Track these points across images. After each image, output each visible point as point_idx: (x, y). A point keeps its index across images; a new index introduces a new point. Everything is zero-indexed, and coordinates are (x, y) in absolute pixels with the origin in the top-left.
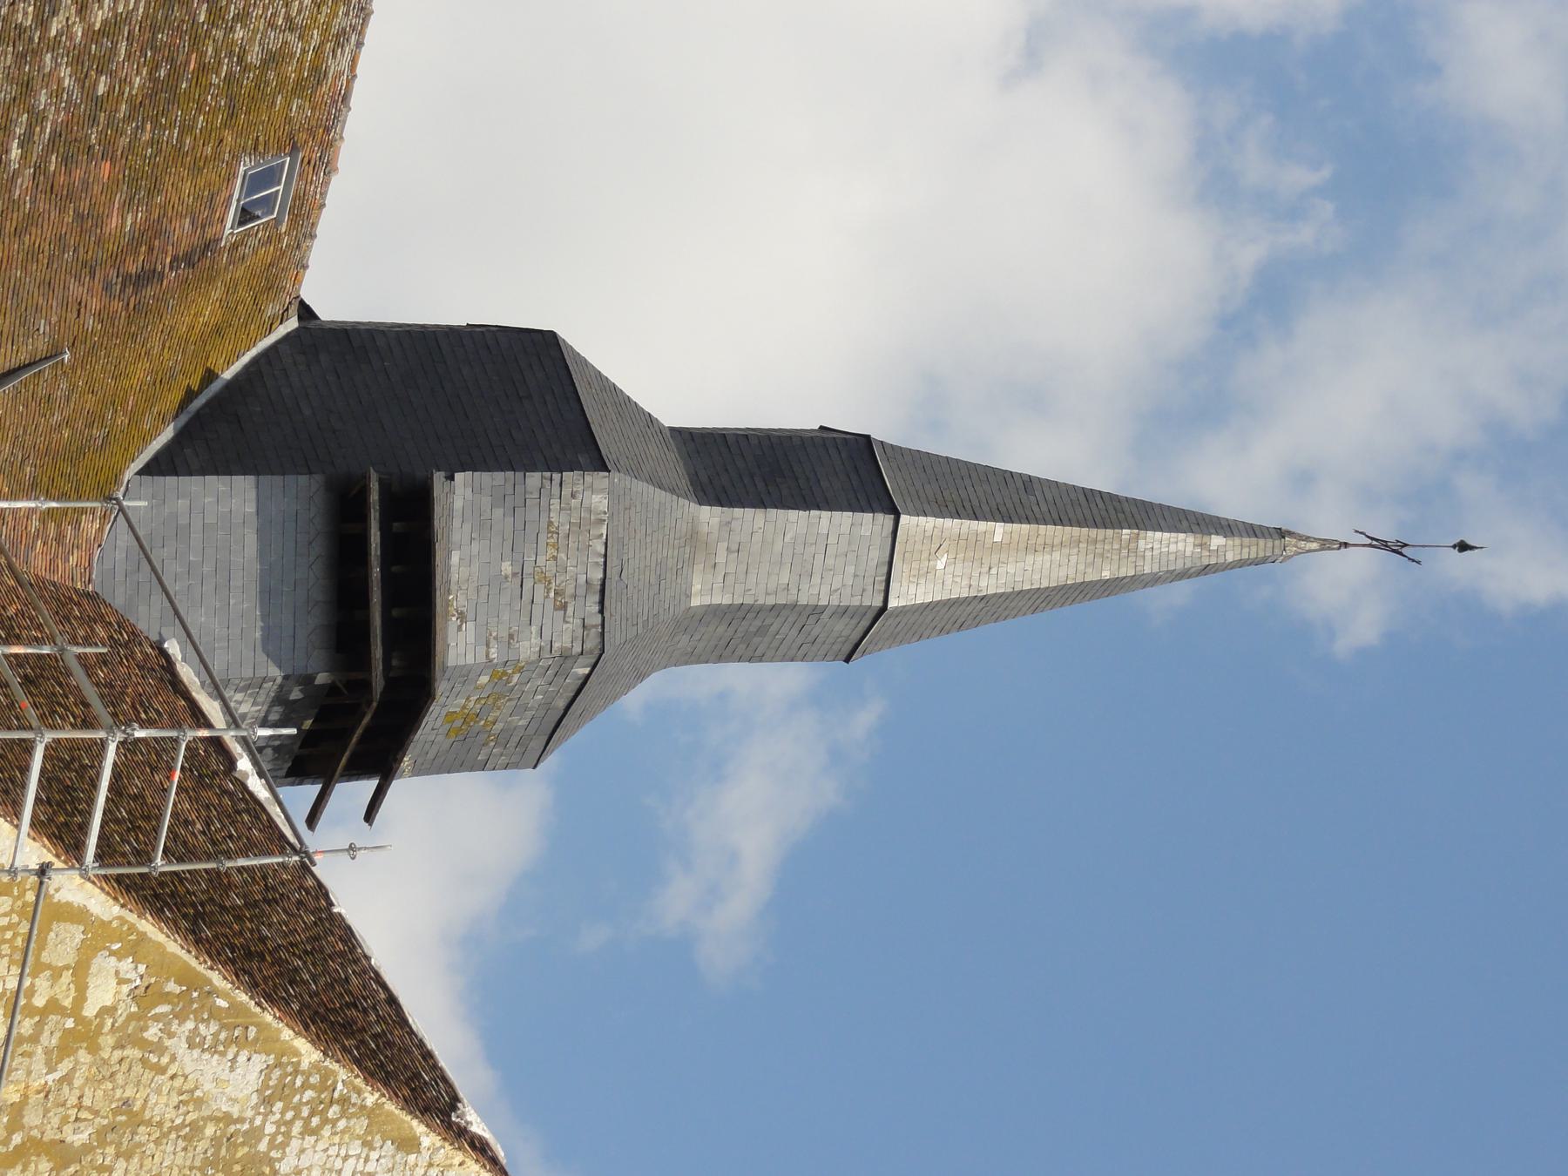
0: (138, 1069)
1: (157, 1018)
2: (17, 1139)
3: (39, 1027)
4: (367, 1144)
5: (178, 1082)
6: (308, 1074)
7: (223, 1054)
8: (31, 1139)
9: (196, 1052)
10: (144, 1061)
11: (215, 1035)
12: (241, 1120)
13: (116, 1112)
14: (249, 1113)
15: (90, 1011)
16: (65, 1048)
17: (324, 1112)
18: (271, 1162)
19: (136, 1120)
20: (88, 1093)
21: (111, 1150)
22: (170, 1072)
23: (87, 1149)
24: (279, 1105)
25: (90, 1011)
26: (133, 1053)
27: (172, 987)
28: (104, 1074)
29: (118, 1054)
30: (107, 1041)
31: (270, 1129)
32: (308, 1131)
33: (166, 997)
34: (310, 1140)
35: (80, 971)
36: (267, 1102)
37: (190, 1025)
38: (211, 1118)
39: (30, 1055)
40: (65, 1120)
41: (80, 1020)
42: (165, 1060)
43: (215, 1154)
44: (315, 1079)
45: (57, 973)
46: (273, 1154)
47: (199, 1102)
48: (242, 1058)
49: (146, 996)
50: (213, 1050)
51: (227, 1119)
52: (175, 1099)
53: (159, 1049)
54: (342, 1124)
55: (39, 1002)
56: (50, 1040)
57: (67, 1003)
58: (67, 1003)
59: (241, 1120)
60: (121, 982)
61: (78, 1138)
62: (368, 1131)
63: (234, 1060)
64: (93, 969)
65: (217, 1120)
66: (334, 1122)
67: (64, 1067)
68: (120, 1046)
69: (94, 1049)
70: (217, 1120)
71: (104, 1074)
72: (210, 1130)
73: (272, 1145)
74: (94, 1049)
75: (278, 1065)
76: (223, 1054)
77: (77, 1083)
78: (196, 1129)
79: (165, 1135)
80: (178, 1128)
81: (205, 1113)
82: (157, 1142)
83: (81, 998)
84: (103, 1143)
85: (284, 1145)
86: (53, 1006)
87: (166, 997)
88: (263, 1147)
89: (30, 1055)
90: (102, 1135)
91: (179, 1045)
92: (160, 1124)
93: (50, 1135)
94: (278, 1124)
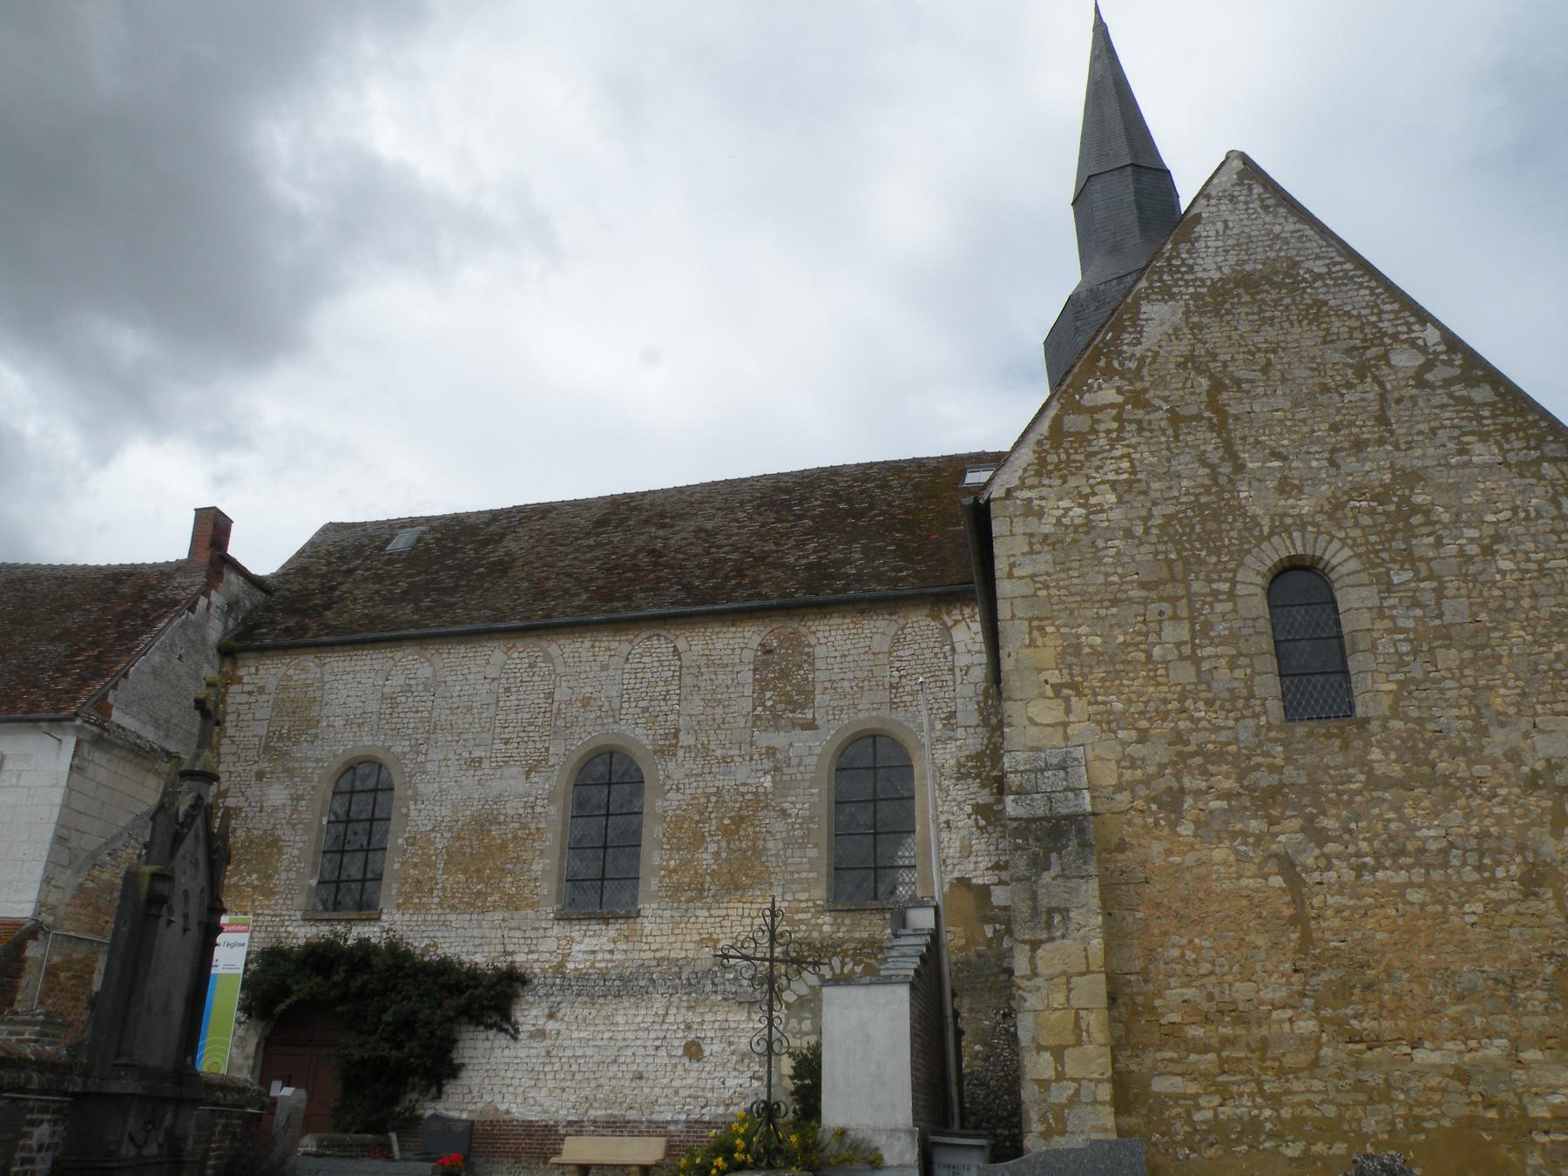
0: (1155, 366)
1: (1122, 364)
2: (1207, 414)
3: (1130, 421)
4: (1197, 240)
5: (1163, 343)
6: (1152, 282)
7: (1142, 326)
8: (1207, 407)
9: (1143, 340)
10: (1150, 364)
11: (1130, 333)
12: (1187, 306)
13: (1186, 368)
14: (1182, 303)
15: (1120, 399)
16: (1147, 405)
17: (1178, 266)
18: (1214, 283)
19: (1191, 357)
20: (1174, 386)
21: (1212, 365)
22: (1157, 349)
23: (1212, 377)
24: (1175, 290)
25: (1120, 399)
26: (1145, 371)
27: (1102, 363)
28: (1162, 382)
29: (1147, 378)
30: (1139, 385)
31: (1191, 290)
32: (1191, 269)
33: (1109, 364)
34: (1196, 268)
35: (1094, 410)
36: (1173, 296)
37: (1125, 348)
38: (1187, 322)
39: (1150, 422)
40: (1192, 394)
41: (1126, 402)
42: (1150, 354)
43: (1210, 312)
44: (1156, 277)
45: (1098, 421)
46: (1209, 283)
47: (1176, 329)
48: (1145, 316)
49: (1109, 373)
50: (1141, 332)
51: (1187, 313)
52: (1175, 342)
53: (1143, 358)
54: (1184, 256)
55: (1115, 425)
56: (1140, 414)
57: (1115, 412)
58: (1115, 412)
59: (1187, 306)
60: (1100, 388)
61: (1204, 383)
62: (1189, 241)
63: (1146, 320)
64: (1092, 404)
65: (1187, 318)
66: (1183, 260)
67: (1157, 402)
68: (1142, 379)
69: (1145, 390)
70: (1187, 318)
71: (1162, 382)
72: (1195, 319)
73: (1204, 285)
74: (1145, 390)
75: (1147, 297)
76: (1142, 326)
77: (1167, 393)
78: (1199, 327)
79: (1200, 341)
80: (1194, 335)
81: (1184, 324)
82: (1206, 343)
83: (1112, 406)
84: (1208, 370)
85: (1202, 280)
86: (1116, 419)
87: (1109, 364)
88: (1204, 290)
89: (1150, 422)
90: (1199, 371)
91: (1138, 351)
92: (1193, 345)
93: (1204, 398)
94: (1187, 286)
